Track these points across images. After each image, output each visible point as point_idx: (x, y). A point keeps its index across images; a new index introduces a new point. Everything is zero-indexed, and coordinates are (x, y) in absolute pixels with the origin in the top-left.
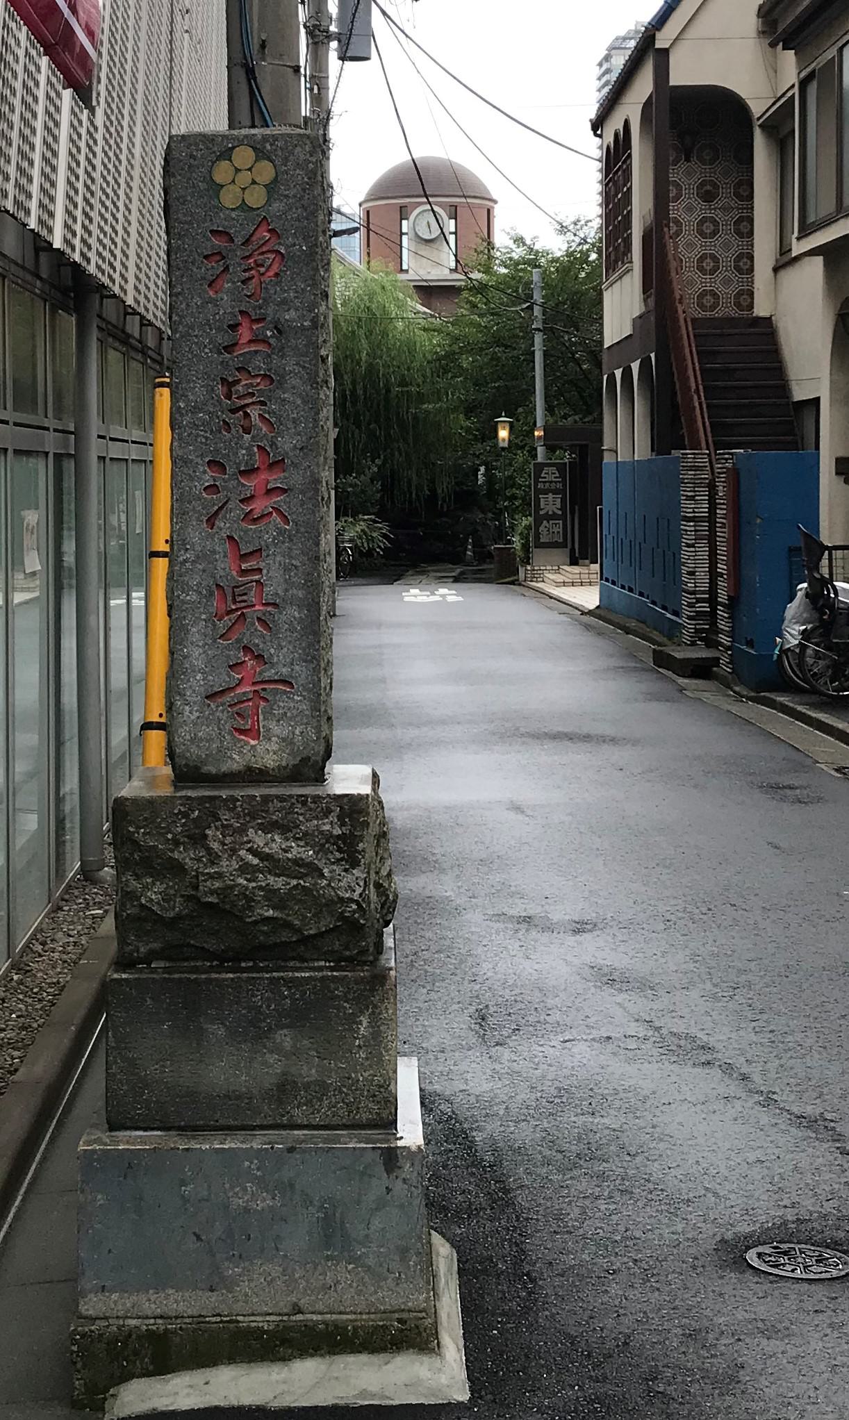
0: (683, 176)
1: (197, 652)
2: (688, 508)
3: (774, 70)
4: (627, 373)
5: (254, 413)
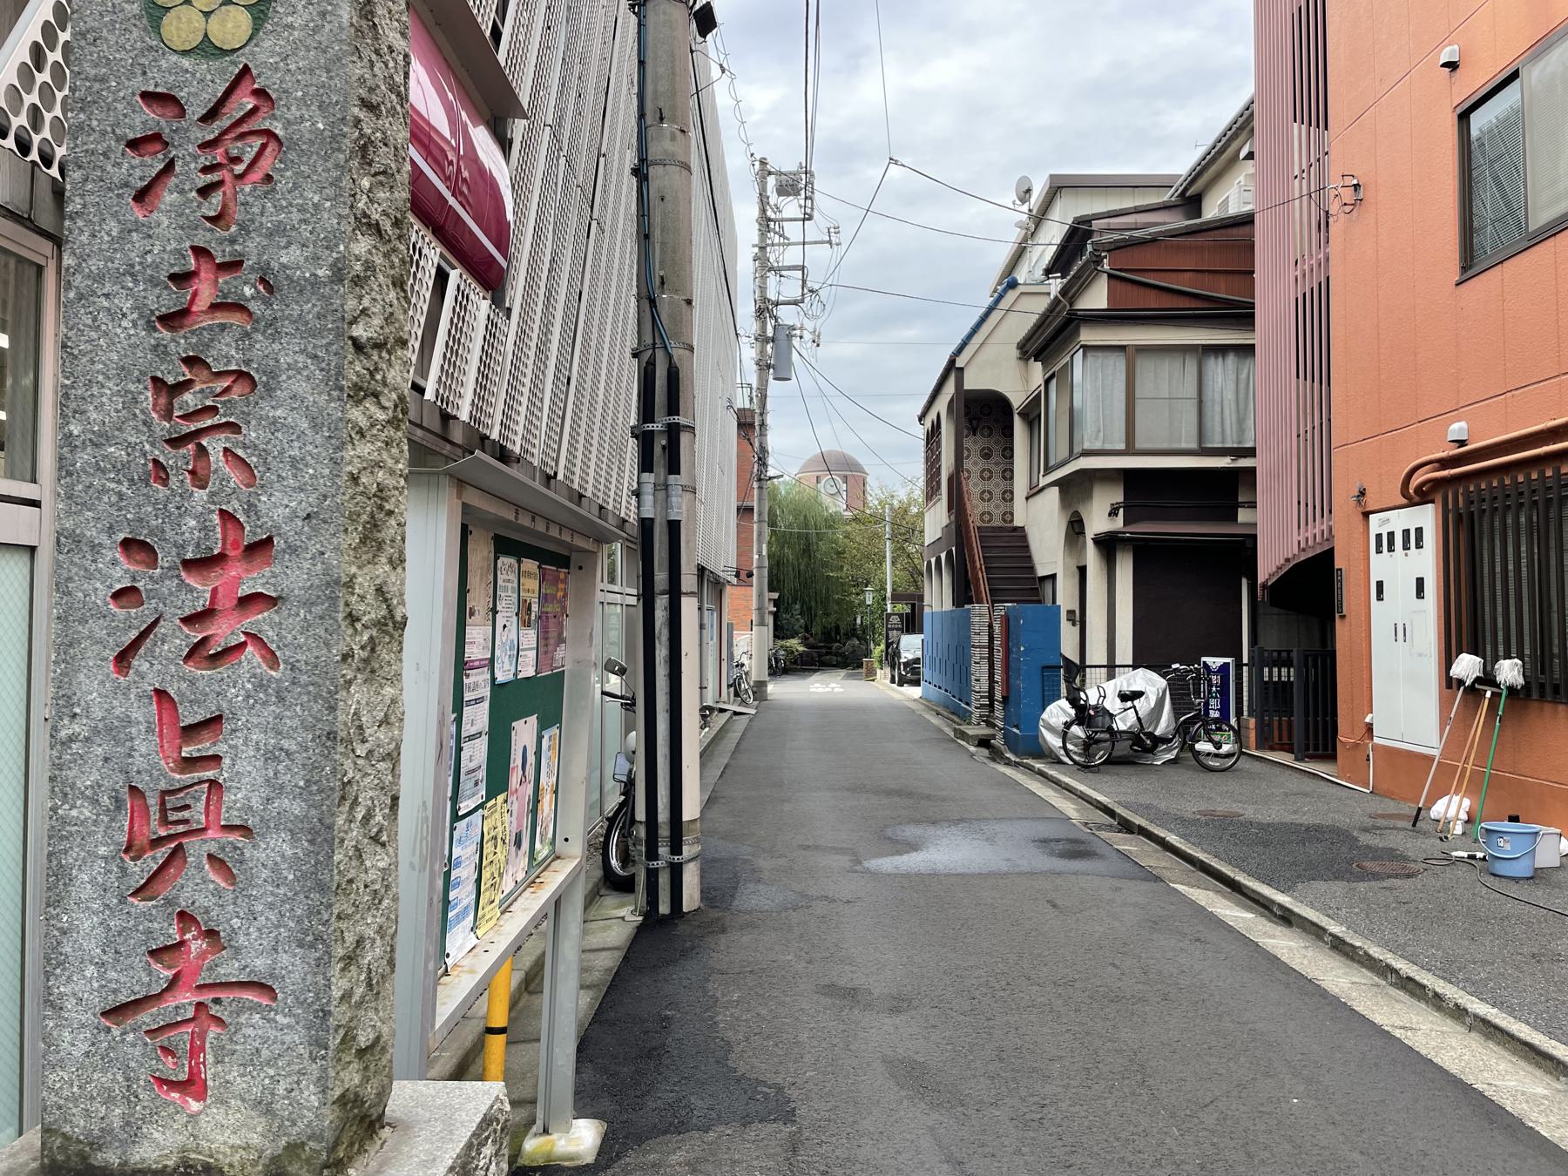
0: (973, 444)
1: (86, 923)
2: (975, 640)
3: (1026, 380)
4: (938, 560)
5: (215, 446)
